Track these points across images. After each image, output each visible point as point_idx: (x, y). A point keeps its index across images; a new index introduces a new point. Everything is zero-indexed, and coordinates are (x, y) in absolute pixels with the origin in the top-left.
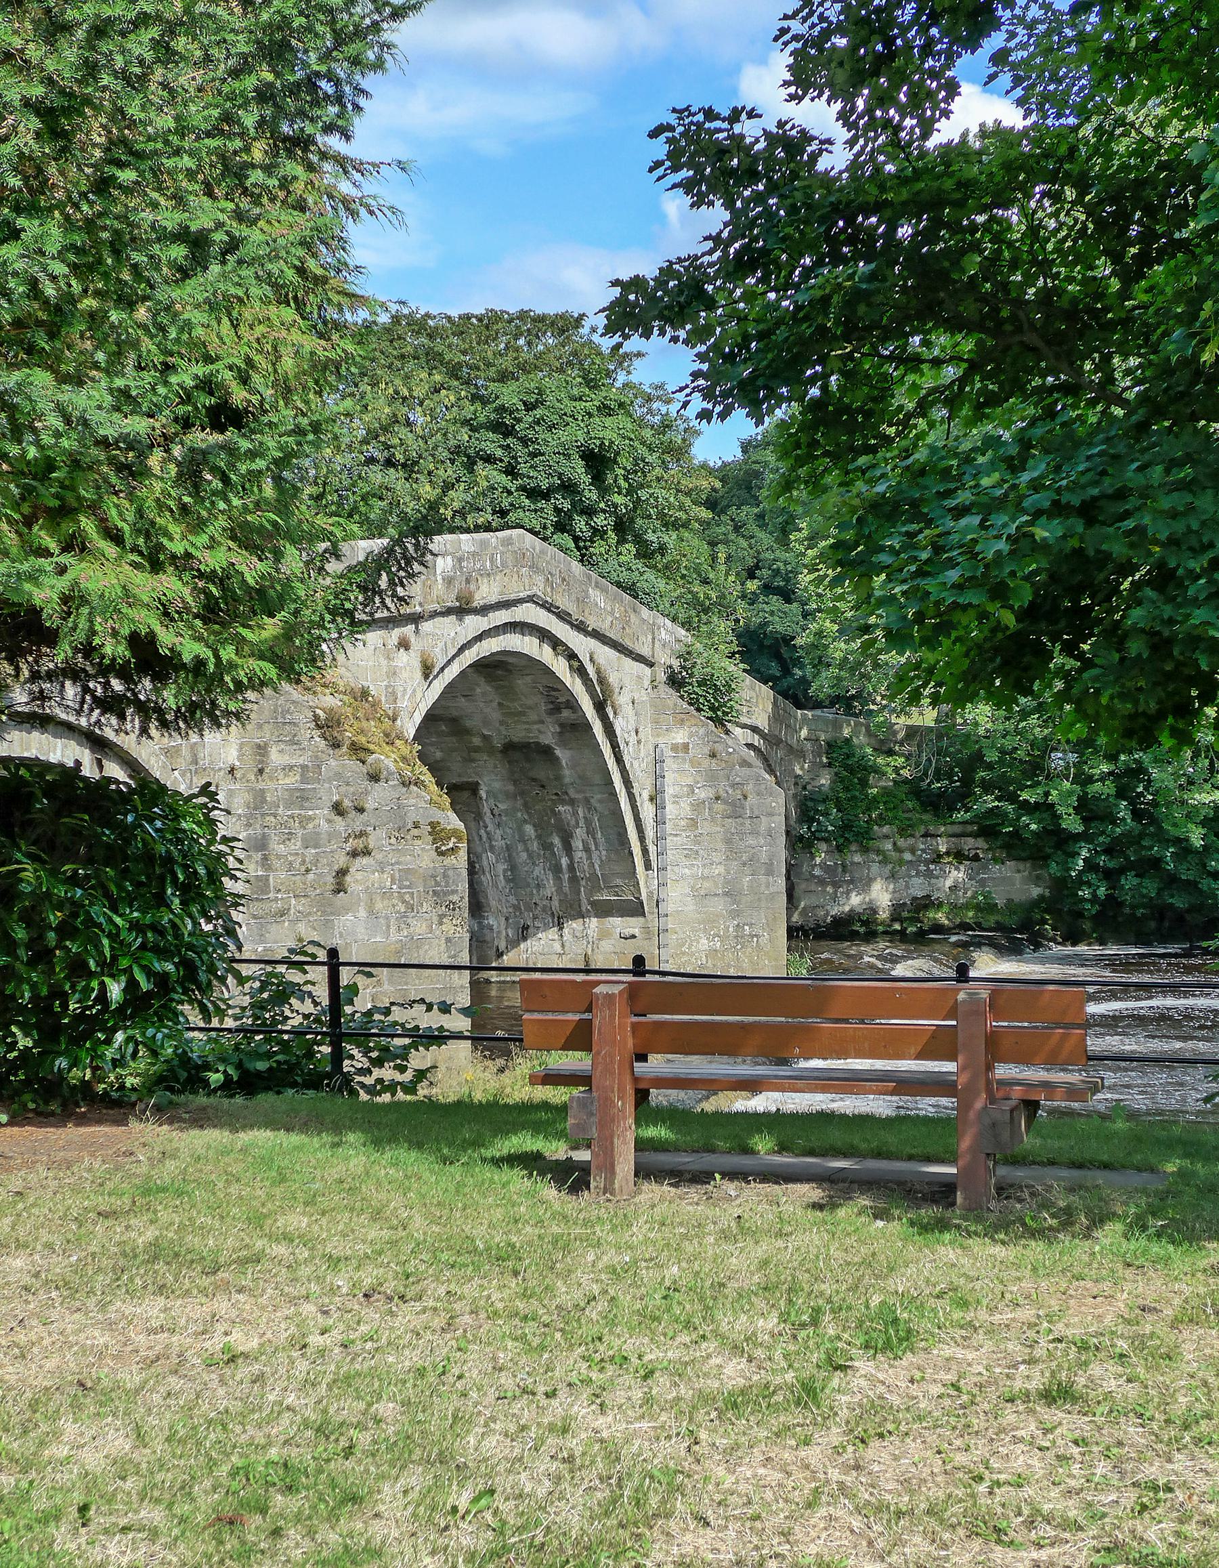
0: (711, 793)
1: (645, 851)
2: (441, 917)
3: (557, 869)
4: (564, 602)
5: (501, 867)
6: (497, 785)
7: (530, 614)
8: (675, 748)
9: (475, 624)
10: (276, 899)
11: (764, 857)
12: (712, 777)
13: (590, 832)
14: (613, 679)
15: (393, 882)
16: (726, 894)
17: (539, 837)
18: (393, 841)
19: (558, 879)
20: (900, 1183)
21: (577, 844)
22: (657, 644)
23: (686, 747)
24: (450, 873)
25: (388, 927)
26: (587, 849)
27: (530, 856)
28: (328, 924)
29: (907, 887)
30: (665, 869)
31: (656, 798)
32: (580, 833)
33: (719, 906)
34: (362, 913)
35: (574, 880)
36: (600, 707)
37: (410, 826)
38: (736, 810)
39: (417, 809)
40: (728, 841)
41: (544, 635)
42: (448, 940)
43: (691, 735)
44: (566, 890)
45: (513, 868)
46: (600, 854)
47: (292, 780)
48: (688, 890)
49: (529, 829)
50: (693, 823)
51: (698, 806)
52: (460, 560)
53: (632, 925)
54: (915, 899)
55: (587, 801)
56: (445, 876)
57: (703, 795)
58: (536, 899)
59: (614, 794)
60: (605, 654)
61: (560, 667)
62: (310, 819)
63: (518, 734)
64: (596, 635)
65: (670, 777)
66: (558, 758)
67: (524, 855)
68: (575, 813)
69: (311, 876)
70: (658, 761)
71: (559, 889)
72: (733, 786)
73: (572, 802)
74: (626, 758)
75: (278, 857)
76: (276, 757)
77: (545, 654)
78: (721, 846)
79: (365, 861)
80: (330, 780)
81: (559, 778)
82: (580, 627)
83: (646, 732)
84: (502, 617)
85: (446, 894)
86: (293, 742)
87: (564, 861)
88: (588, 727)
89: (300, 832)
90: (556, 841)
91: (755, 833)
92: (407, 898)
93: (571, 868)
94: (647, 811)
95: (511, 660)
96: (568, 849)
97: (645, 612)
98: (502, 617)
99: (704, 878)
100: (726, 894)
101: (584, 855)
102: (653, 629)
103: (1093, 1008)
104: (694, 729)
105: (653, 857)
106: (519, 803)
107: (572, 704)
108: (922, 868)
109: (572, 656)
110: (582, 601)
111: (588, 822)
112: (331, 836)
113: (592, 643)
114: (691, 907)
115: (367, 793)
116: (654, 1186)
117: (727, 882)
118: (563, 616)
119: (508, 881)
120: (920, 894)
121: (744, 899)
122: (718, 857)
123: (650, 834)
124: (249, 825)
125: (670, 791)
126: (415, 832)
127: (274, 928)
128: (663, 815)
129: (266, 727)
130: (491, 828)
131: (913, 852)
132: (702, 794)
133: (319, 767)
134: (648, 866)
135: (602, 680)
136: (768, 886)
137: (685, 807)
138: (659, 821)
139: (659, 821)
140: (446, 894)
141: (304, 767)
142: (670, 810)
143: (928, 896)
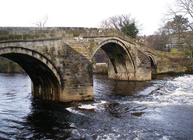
21: (126, 65)
41: (118, 41)
77: (119, 43)
84: (111, 38)
102: (135, 41)
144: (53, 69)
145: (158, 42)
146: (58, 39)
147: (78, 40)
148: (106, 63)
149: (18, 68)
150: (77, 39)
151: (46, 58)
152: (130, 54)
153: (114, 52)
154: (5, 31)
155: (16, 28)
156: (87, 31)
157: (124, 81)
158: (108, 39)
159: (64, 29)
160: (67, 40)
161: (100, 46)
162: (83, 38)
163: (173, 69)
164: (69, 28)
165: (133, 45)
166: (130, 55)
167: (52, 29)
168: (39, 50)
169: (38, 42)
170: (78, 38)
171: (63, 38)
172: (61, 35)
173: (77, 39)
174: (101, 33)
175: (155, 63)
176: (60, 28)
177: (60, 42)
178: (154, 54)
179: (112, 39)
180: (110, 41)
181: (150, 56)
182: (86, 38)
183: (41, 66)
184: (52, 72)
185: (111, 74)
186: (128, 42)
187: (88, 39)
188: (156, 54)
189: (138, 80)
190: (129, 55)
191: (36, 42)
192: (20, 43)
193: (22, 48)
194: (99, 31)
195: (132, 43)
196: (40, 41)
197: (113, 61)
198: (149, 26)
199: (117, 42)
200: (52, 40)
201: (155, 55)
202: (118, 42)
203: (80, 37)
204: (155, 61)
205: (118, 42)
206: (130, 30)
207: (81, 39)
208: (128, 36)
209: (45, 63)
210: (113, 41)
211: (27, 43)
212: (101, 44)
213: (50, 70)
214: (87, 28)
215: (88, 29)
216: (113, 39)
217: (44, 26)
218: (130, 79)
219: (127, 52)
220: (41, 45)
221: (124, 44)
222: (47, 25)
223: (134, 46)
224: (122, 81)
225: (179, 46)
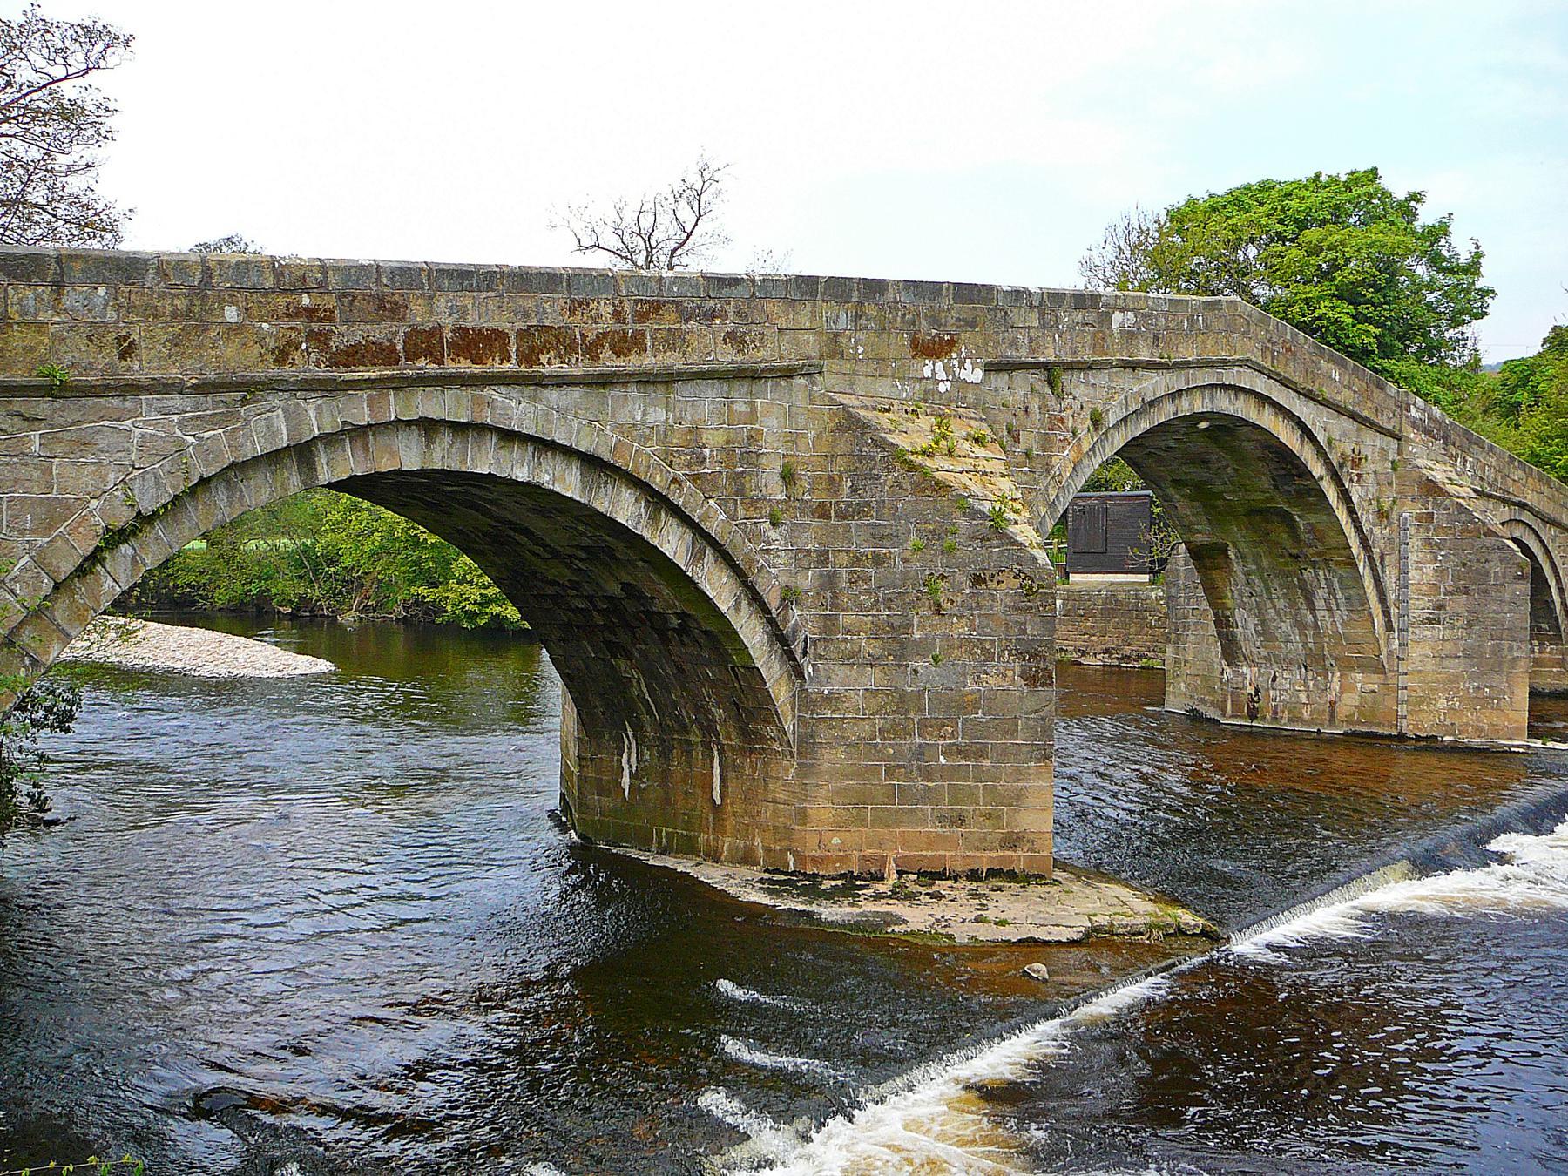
4: (1289, 372)
5: (1251, 622)
13: (1332, 592)
21: (1320, 604)
32: (1321, 593)
41: (1263, 400)
46: (1342, 613)
53: (1373, 682)
71: (1305, 644)
77: (1267, 420)
82: (1309, 395)
84: (1207, 377)
96: (1313, 609)
98: (1207, 377)
103: (732, 1047)
107: (1305, 473)
109: (1300, 424)
110: (1311, 372)
111: (1329, 585)
114: (1430, 665)
116: (933, 1068)
118: (1285, 383)
128: (1406, 579)
137: (1429, 569)
139: (1403, 586)
173: (941, 375)
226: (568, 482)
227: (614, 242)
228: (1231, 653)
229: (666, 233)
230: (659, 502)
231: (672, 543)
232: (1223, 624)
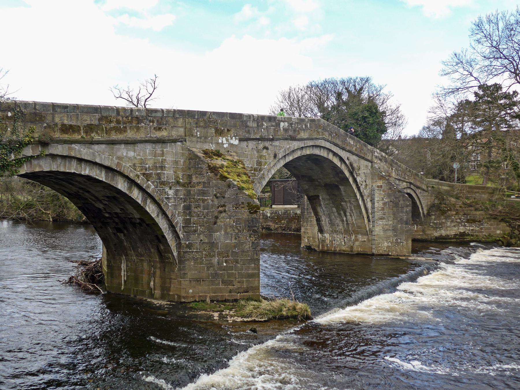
0: (389, 200)
1: (368, 217)
2: (250, 235)
3: (343, 221)
6: (324, 196)
7: (323, 143)
8: (378, 187)
9: (295, 145)
10: (193, 227)
11: (405, 219)
12: (389, 196)
13: (351, 210)
14: (355, 165)
15: (234, 222)
16: (393, 230)
17: (337, 211)
18: (234, 208)
19: (343, 224)
20: (477, 290)
21: (348, 214)
22: (373, 157)
23: (381, 186)
24: (254, 220)
25: (232, 237)
26: (351, 216)
27: (335, 217)
28: (211, 236)
29: (458, 229)
30: (374, 222)
31: (372, 201)
32: (348, 210)
33: (390, 233)
34: (223, 233)
35: (348, 224)
36: (351, 173)
37: (240, 203)
38: (396, 205)
39: (243, 198)
40: (394, 214)
41: (330, 150)
42: (253, 243)
43: (383, 183)
44: (345, 227)
45: (331, 220)
47: (200, 187)
48: (381, 228)
49: (334, 209)
50: (383, 209)
51: (385, 204)
52: (291, 124)
54: (460, 233)
55: (350, 201)
56: (252, 221)
57: (386, 201)
58: (337, 229)
59: (357, 200)
60: (353, 158)
61: (336, 161)
62: (206, 200)
63: (328, 181)
64: (349, 151)
65: (376, 195)
66: (340, 189)
67: (333, 217)
68: (347, 205)
69: (205, 219)
70: (373, 190)
71: (344, 226)
72: (395, 198)
73: (345, 202)
74: (361, 189)
75: (194, 212)
76: (194, 180)
77: (331, 157)
78: (392, 216)
79: (224, 214)
80: (213, 187)
81: (341, 194)
83: (369, 182)
84: (311, 143)
85: (252, 227)
86: (200, 174)
87: (345, 219)
88: (347, 179)
89: (202, 204)
90: (342, 212)
91: (402, 212)
92: (239, 228)
93: (347, 221)
94: (369, 205)
95: (319, 158)
96: (346, 216)
97: (369, 147)
99: (386, 225)
100: (393, 230)
101: (350, 217)
102: (373, 152)
104: (384, 181)
105: (371, 218)
106: (331, 202)
108: (463, 224)
112: (213, 206)
113: (349, 154)
114: (382, 233)
115: (226, 192)
117: (393, 226)
119: (329, 224)
120: (462, 231)
121: (398, 232)
122: (391, 219)
123: (370, 211)
124: (185, 201)
125: (376, 199)
126: (242, 206)
127: (192, 236)
129: (192, 169)
130: (324, 208)
131: (460, 219)
132: (386, 200)
133: (209, 183)
134: (369, 221)
135: (351, 164)
136: (406, 228)
137: (381, 203)
138: (373, 208)
139: (373, 208)
140: (252, 227)
141: (204, 182)
142: (376, 205)
143: (464, 232)
144: (158, 215)
145: (438, 156)
146: (175, 141)
147: (225, 146)
148: (296, 206)
149: (73, 211)
150: (225, 142)
151: (140, 188)
152: (357, 185)
153: (316, 180)
154: (35, 114)
155: (54, 107)
156: (250, 124)
157: (341, 254)
158: (303, 146)
159: (190, 114)
160: (199, 145)
161: (282, 163)
162: (241, 140)
163: (471, 228)
164: (203, 114)
165: (366, 163)
166: (359, 189)
167: (159, 115)
168: (126, 168)
169: (123, 146)
170: (227, 140)
171: (187, 138)
172: (182, 130)
173: (225, 142)
174: (286, 130)
175: (422, 209)
176: (182, 113)
177: (179, 148)
178: (418, 188)
179: (313, 146)
180: (308, 152)
181: (409, 191)
182: (247, 140)
183: (130, 209)
184: (156, 224)
185: (310, 234)
186: (353, 154)
187: (252, 144)
188: (427, 187)
189: (375, 251)
190: (354, 187)
191: (117, 146)
192: (73, 146)
193: (80, 160)
194: (282, 124)
195: (363, 158)
196: (127, 143)
197: (313, 200)
198: (415, 108)
199: (325, 155)
200: (160, 142)
201: (424, 190)
202: (130, 189)
203: (232, 138)
204: (424, 206)
205: (328, 154)
206: (358, 115)
207: (236, 142)
208: (353, 139)
209: (139, 201)
210: (317, 152)
211: (93, 146)
212: (285, 156)
213: (153, 219)
214: (249, 116)
215: (254, 120)
216: (317, 146)
217: (147, 107)
218: (355, 249)
219: (351, 180)
220: (131, 154)
221: (341, 159)
222: (152, 105)
223: (370, 164)
224: (335, 253)
225: (489, 168)
226: (102, 176)
227: (126, 96)
228: (321, 231)
229: (144, 95)
230: (132, 182)
231: (136, 195)
232: (318, 220)
